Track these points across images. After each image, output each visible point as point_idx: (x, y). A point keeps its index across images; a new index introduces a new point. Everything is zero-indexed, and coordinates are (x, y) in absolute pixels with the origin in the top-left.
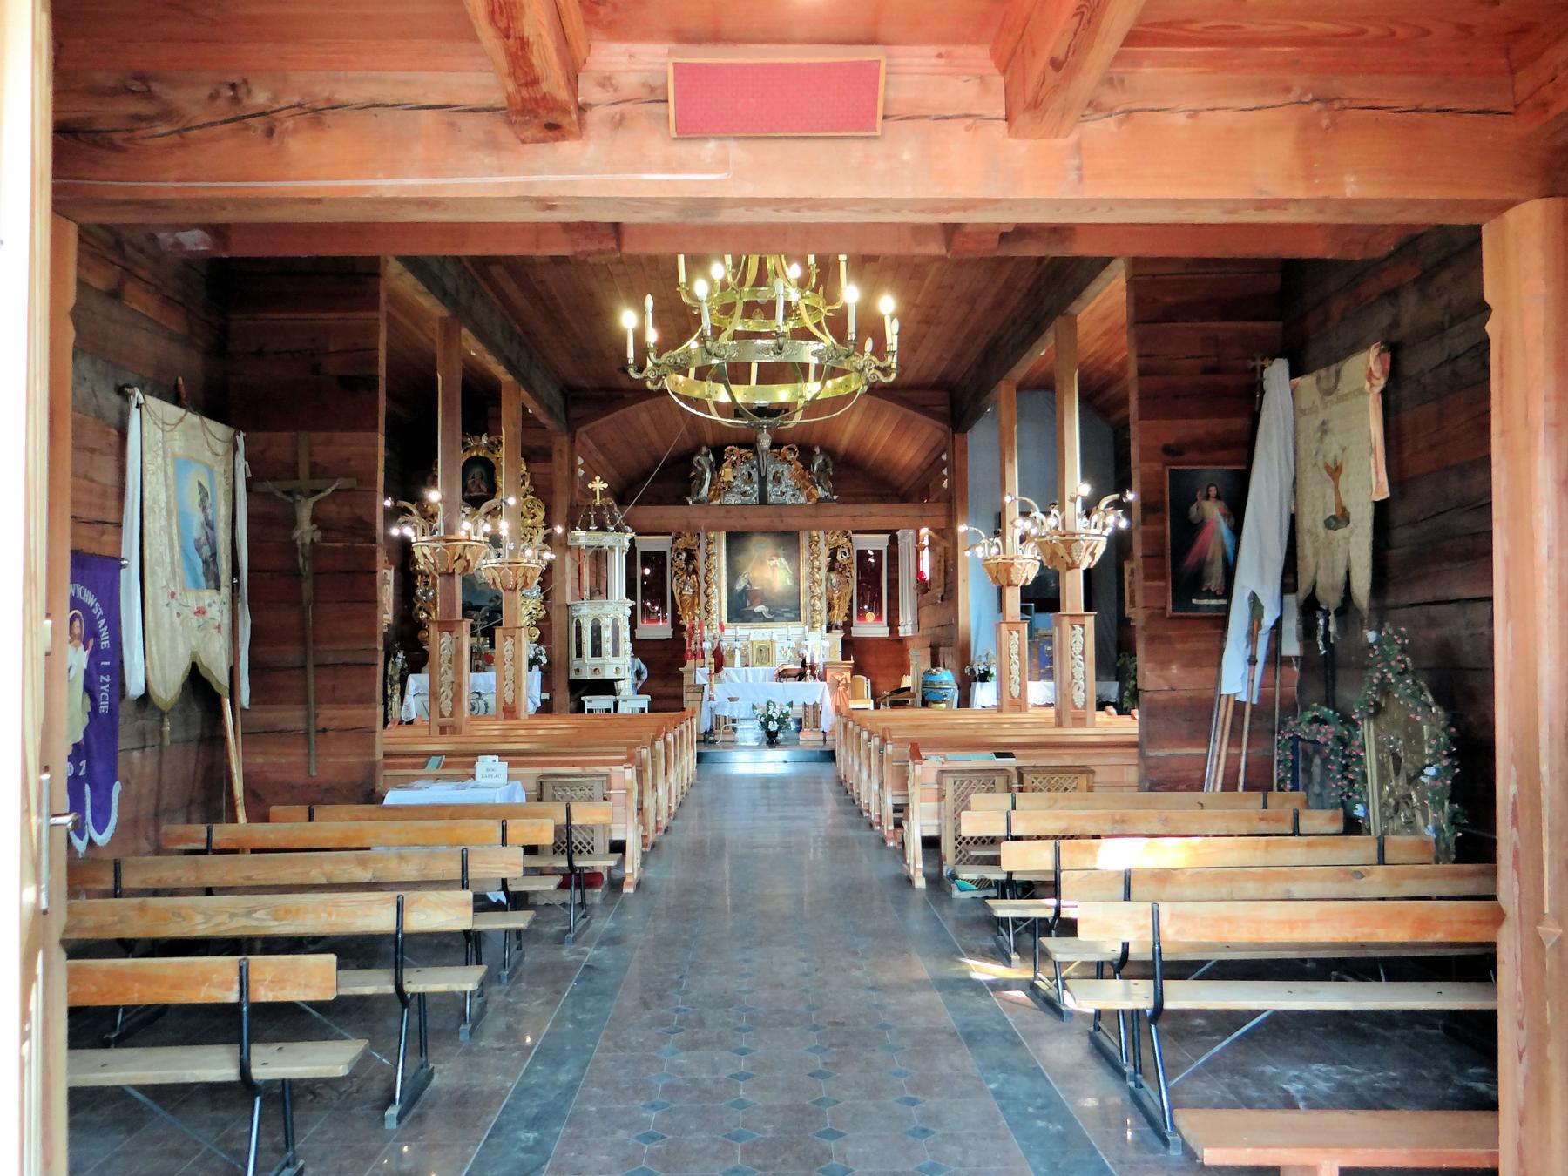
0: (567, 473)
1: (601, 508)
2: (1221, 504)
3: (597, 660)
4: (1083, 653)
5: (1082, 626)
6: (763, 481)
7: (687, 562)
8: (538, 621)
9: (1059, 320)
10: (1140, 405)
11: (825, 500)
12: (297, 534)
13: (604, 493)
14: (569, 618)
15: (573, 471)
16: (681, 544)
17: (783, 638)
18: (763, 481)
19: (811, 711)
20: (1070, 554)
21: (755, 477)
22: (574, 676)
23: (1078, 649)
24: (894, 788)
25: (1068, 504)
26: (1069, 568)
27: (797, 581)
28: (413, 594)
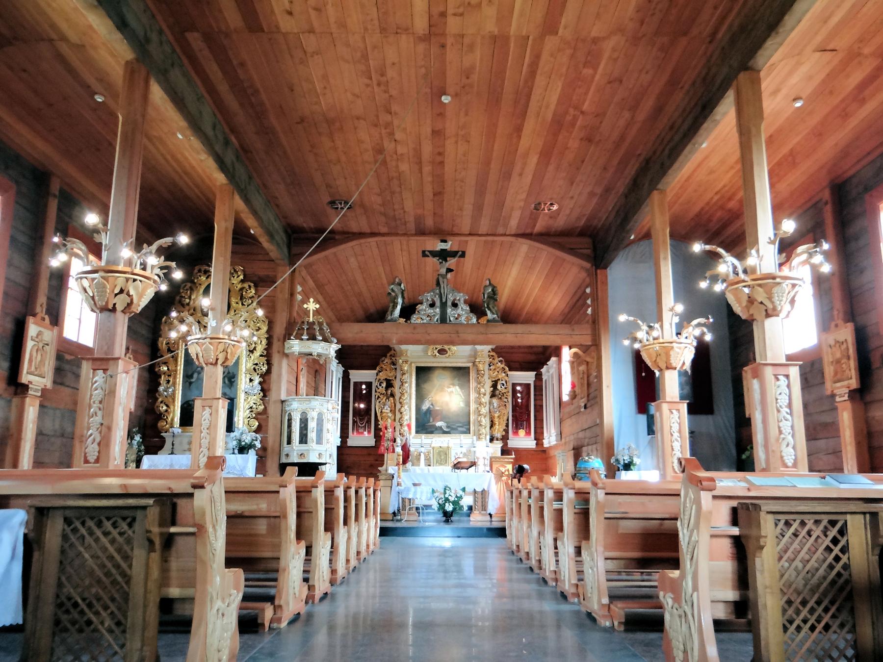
0: (287, 296)
1: (314, 323)
3: (303, 447)
4: (790, 406)
6: (444, 305)
7: (387, 388)
8: (259, 414)
9: (742, 76)
10: (413, 630)
11: (494, 320)
13: (317, 312)
14: (283, 411)
15: (292, 294)
16: (382, 376)
17: (457, 445)
18: (444, 305)
19: (479, 496)
20: (770, 298)
21: (438, 303)
23: (784, 400)
24: (607, 548)
26: (768, 315)
27: (468, 404)
28: (157, 391)
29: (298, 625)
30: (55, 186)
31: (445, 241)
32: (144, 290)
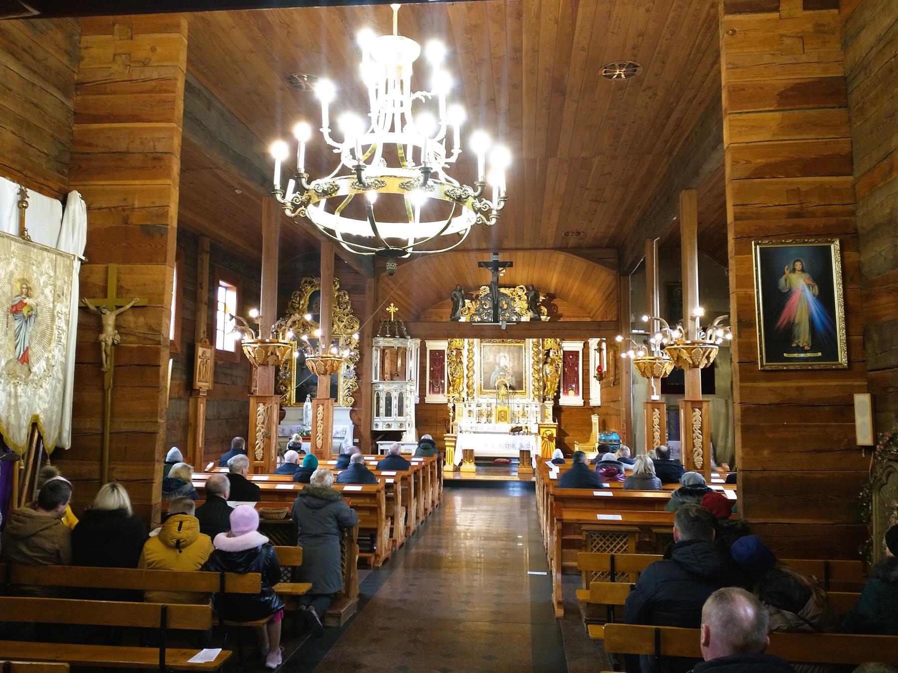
1: (394, 323)
2: (806, 276)
3: (388, 419)
5: (700, 409)
8: (355, 392)
10: (736, 243)
12: (102, 337)
22: (375, 429)
25: (690, 322)
29: (388, 564)
30: (206, 244)
31: (497, 254)
32: (285, 351)
